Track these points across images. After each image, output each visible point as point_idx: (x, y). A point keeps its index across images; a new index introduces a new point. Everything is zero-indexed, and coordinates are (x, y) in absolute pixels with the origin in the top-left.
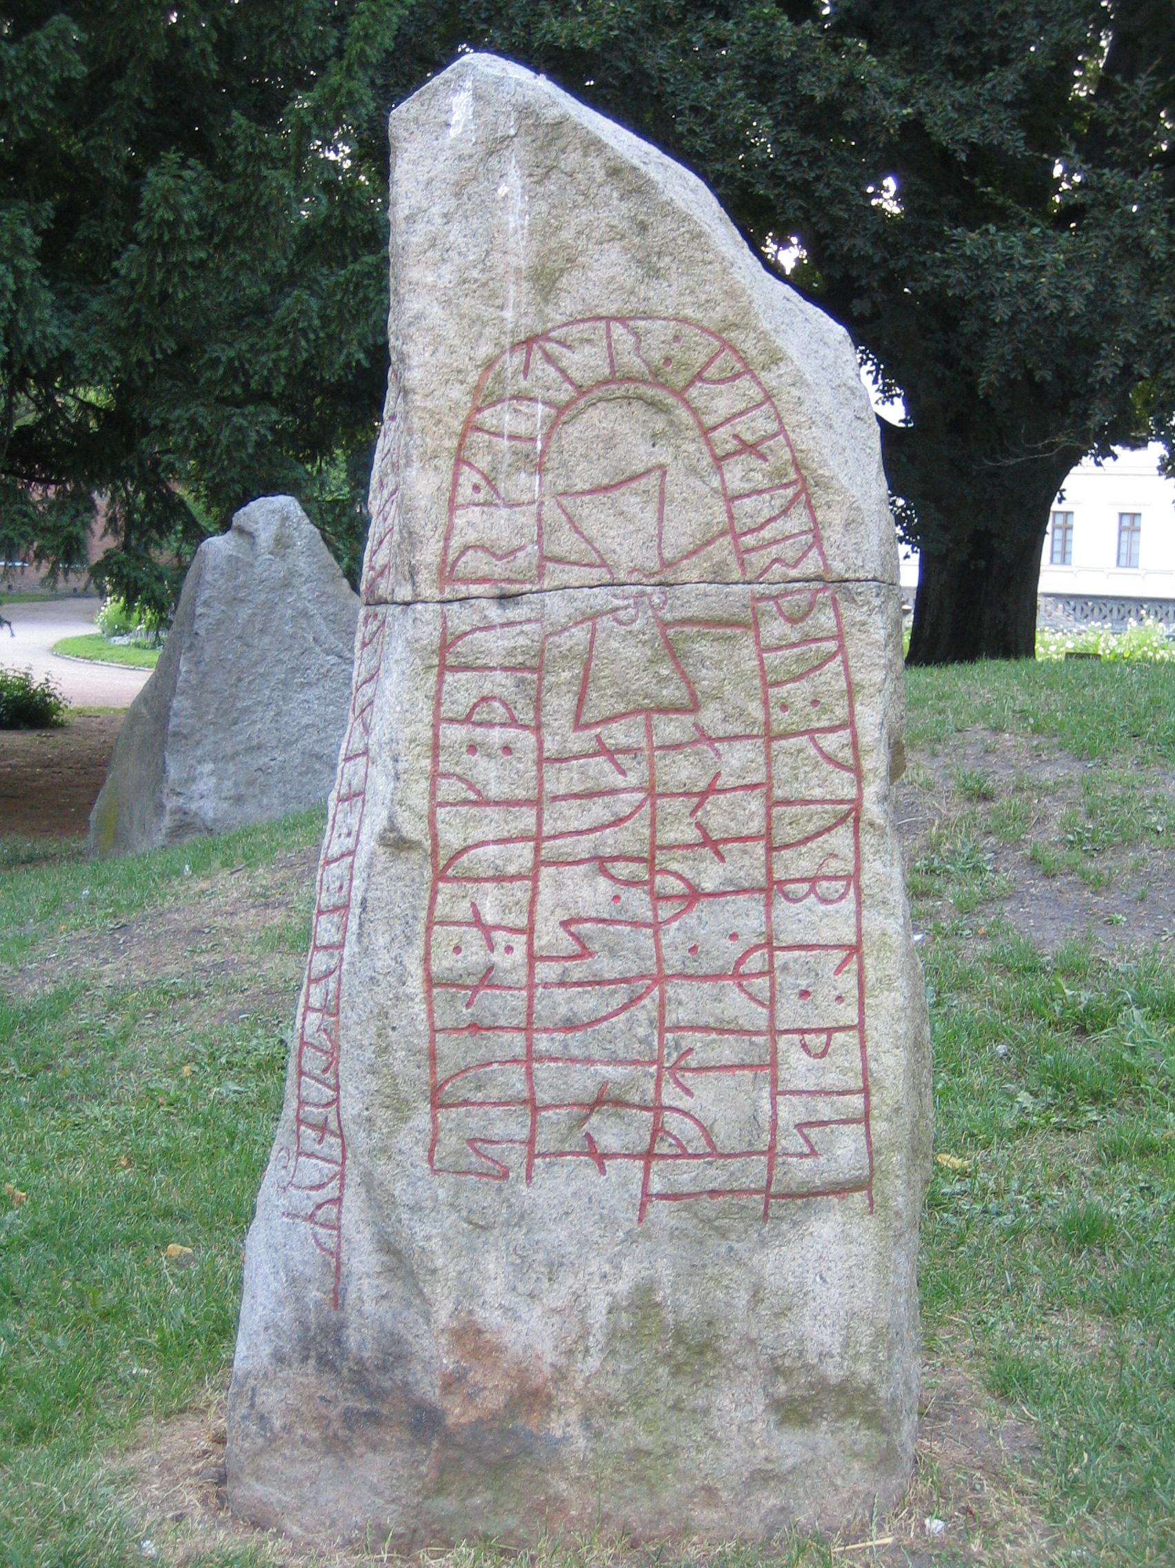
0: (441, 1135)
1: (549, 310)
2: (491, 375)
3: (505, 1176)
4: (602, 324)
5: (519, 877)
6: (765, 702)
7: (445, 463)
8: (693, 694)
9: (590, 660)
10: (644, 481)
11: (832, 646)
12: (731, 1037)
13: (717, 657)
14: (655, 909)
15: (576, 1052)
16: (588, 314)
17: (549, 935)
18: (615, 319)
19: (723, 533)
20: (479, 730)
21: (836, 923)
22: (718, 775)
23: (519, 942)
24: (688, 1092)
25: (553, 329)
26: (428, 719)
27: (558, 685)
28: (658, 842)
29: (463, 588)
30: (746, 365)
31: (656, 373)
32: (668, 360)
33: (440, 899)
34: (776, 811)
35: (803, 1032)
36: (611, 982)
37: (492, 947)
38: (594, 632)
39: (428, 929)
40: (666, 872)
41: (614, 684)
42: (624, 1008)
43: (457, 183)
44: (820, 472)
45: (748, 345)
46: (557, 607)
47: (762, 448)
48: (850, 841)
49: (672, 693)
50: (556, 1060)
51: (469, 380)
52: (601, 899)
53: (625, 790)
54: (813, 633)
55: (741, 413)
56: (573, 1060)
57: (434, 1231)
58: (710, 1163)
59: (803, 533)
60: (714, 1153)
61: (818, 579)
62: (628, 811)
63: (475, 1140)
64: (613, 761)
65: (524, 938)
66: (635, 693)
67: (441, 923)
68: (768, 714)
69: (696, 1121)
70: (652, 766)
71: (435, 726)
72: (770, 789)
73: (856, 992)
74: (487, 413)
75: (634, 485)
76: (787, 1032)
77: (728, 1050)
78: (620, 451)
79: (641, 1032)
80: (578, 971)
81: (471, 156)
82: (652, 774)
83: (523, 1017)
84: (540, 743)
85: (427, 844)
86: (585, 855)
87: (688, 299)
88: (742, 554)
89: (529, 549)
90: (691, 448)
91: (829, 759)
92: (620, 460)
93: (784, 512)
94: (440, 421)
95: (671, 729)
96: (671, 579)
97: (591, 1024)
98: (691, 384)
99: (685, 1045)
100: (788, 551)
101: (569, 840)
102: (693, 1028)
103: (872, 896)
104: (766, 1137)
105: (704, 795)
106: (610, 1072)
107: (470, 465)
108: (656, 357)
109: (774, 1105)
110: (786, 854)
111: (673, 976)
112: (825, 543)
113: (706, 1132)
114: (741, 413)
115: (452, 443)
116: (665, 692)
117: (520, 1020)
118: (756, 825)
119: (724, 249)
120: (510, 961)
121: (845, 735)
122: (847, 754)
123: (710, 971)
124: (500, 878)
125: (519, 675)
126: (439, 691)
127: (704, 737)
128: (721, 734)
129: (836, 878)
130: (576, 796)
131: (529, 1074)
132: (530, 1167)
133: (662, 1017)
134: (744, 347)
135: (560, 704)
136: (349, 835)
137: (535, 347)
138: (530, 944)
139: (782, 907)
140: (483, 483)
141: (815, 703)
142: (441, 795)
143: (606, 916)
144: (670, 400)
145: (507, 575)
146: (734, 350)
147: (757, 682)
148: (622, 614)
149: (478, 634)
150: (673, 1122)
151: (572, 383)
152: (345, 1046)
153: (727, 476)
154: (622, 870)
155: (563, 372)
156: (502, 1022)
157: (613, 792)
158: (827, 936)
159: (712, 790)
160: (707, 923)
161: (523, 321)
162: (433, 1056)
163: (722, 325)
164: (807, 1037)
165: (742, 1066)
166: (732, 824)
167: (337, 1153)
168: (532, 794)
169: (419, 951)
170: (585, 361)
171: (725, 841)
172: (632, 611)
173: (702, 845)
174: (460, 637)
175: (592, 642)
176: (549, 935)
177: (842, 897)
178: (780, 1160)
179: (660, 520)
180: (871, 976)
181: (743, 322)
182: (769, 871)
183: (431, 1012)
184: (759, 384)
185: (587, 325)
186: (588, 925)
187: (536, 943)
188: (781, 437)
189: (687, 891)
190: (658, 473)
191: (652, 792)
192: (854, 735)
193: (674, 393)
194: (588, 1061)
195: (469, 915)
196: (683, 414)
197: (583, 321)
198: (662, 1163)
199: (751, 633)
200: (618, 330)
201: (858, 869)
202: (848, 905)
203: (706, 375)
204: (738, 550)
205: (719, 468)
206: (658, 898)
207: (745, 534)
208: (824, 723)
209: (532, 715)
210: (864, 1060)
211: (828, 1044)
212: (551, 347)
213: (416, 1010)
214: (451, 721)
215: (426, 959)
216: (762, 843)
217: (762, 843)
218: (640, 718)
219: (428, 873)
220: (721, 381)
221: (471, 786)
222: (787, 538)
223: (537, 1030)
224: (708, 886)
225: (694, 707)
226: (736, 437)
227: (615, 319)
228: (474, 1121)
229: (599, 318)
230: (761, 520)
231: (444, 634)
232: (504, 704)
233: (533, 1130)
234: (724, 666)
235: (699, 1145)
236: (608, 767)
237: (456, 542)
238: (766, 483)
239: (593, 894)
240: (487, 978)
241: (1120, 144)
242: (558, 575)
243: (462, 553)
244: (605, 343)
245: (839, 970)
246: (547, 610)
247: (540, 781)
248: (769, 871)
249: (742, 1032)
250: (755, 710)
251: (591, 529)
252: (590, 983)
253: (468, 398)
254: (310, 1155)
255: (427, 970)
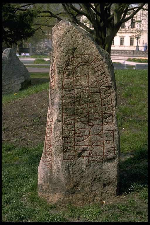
136: (51, 119)
152: (52, 145)
167: (51, 158)
194: (82, 145)
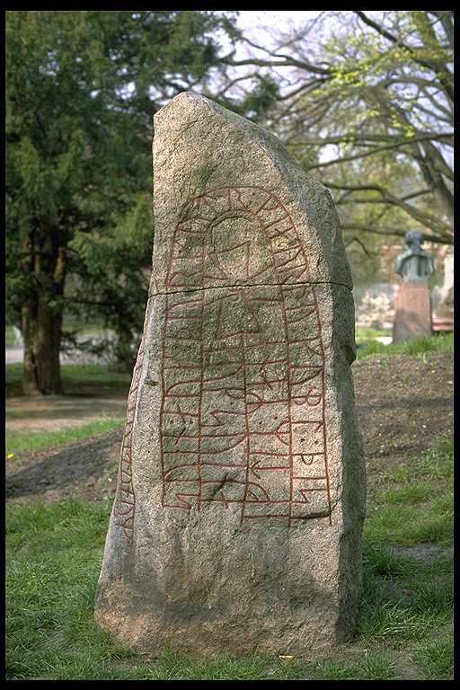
7: (169, 242)
11: (313, 307)
56: (216, 464)
133: (249, 448)
158: (311, 417)
160: (265, 412)
167: (132, 500)
194: (221, 465)
198: (250, 505)
224: (266, 399)
240: (183, 433)
241: (117, 62)
254: (125, 502)
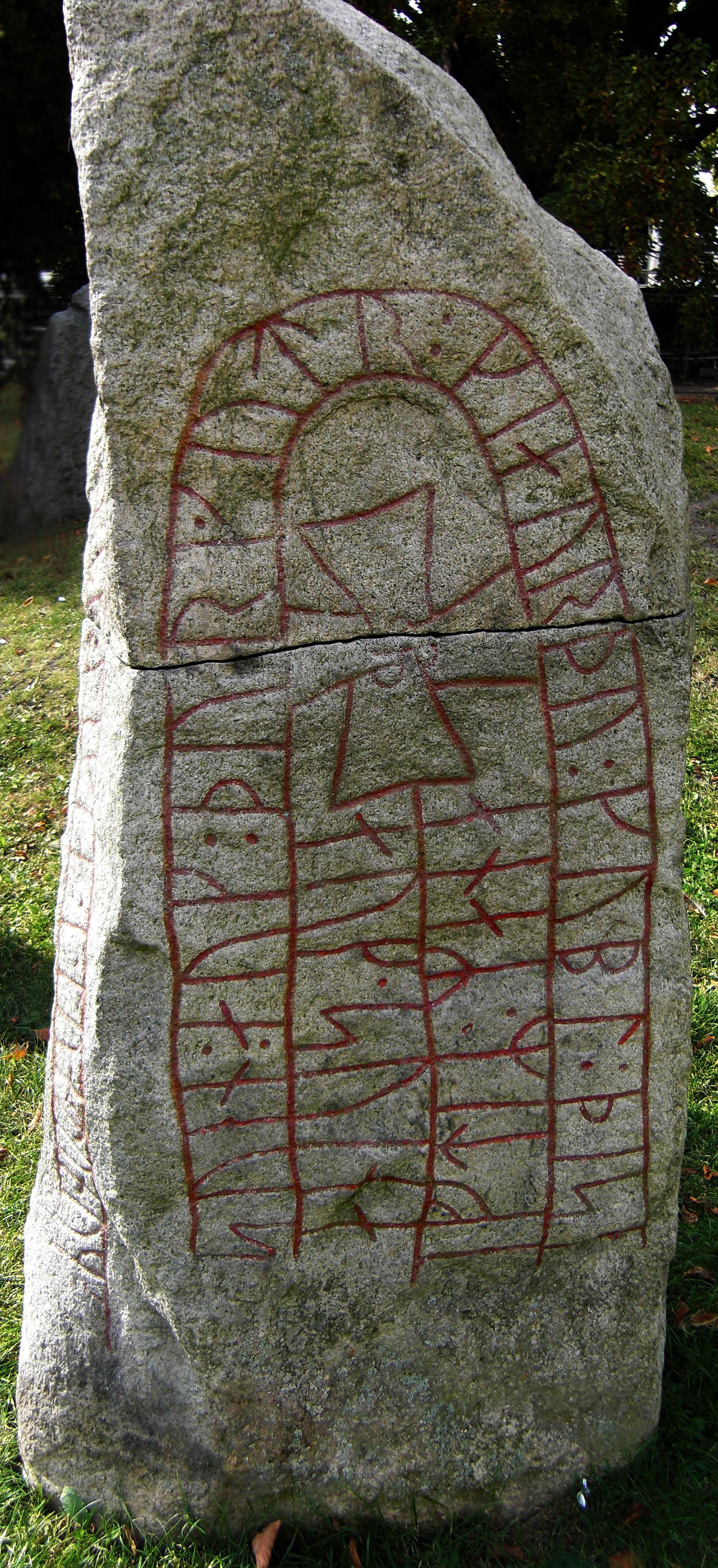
0: (202, 1224)
1: (282, 283)
2: (212, 375)
3: (272, 1253)
4: (352, 300)
5: (273, 971)
6: (552, 767)
7: (160, 492)
8: (468, 760)
9: (346, 731)
10: (406, 504)
11: (630, 697)
12: (507, 1110)
13: (497, 719)
14: (425, 990)
15: (340, 1135)
16: (333, 286)
17: (310, 1023)
18: (367, 292)
19: (504, 569)
20: (218, 817)
21: (622, 990)
22: (498, 850)
23: (276, 1036)
24: (462, 1165)
25: (289, 308)
26: (157, 809)
27: (310, 761)
28: (429, 923)
29: (190, 651)
30: (534, 352)
31: (421, 363)
32: (436, 347)
33: (184, 1001)
34: (561, 884)
35: (582, 1099)
36: (377, 1064)
37: (245, 1043)
38: (349, 697)
39: (174, 1034)
40: (437, 949)
41: (376, 756)
42: (393, 1087)
43: (154, 106)
44: (624, 490)
45: (540, 329)
46: (305, 667)
47: (554, 460)
48: (640, 906)
49: (444, 761)
50: (321, 1145)
51: (184, 382)
52: (364, 984)
53: (389, 872)
54: (609, 684)
55: (528, 416)
57: (200, 1314)
58: (484, 1227)
59: (599, 562)
60: (489, 1215)
61: (619, 619)
62: (394, 894)
63: (239, 1224)
64: (377, 841)
65: (281, 1030)
66: (400, 764)
67: (188, 1025)
68: (555, 781)
69: (472, 1192)
70: (421, 844)
71: (166, 817)
72: (556, 859)
73: (640, 1060)
74: (208, 424)
75: (395, 509)
76: (565, 1102)
77: (503, 1122)
78: (376, 468)
79: (412, 1113)
80: (343, 1056)
81: (171, 65)
82: (422, 854)
83: (284, 1107)
84: (290, 826)
85: (166, 947)
86: (346, 942)
87: (461, 264)
88: (527, 594)
89: (268, 597)
90: (464, 460)
91: (622, 823)
92: (378, 478)
93: (579, 537)
94: (148, 438)
95: (443, 801)
96: (442, 629)
97: (357, 1105)
98: (465, 377)
99: (458, 1123)
100: (581, 585)
101: (327, 930)
102: (466, 1106)
103: (661, 961)
104: (543, 1201)
105: (480, 872)
106: (377, 1153)
107: (190, 492)
108: (421, 342)
109: (551, 1172)
110: (570, 925)
111: (445, 1056)
112: (626, 574)
113: (481, 1200)
114: (528, 416)
115: (166, 466)
116: (435, 762)
117: (281, 1109)
118: (539, 900)
119: (505, 194)
120: (268, 1052)
121: (642, 797)
122: (642, 819)
123: (485, 1049)
124: (250, 974)
125: (263, 752)
126: (168, 774)
127: (481, 808)
128: (500, 804)
129: (623, 944)
130: (337, 880)
131: (293, 1160)
132: (297, 1243)
134: (533, 328)
135: (312, 785)
137: (266, 332)
138: (288, 1035)
139: (565, 980)
140: (208, 515)
141: (609, 763)
142: (177, 894)
143: (372, 1001)
144: (439, 399)
145: (243, 631)
146: (521, 334)
147: (543, 745)
148: (384, 674)
149: (211, 708)
150: (445, 1194)
151: (315, 381)
153: (510, 495)
154: (387, 952)
155: (302, 365)
156: (261, 1114)
157: (378, 874)
158: (613, 1007)
159: (489, 866)
161: (249, 299)
162: (187, 1157)
163: (504, 299)
164: (587, 1104)
165: (518, 1136)
166: (512, 900)
168: (282, 884)
169: (164, 1058)
170: (332, 351)
171: (503, 916)
172: (396, 669)
173: (479, 921)
174: (188, 712)
175: (348, 711)
176: (310, 1023)
177: (629, 964)
178: (557, 1220)
179: (428, 552)
180: (657, 1042)
181: (534, 295)
182: (551, 942)
183: (181, 1117)
184: (551, 377)
185: (332, 301)
186: (352, 1012)
187: (295, 1034)
188: (577, 446)
189: (460, 967)
190: (424, 494)
191: (421, 870)
192: (652, 797)
193: (444, 388)
194: (355, 1143)
195: (219, 1016)
196: (455, 417)
197: (327, 295)
199: (537, 689)
200: (372, 308)
201: (648, 933)
202: (634, 974)
203: (484, 365)
204: (522, 587)
205: (500, 484)
206: (427, 976)
207: (531, 569)
208: (619, 784)
209: (279, 796)
210: (646, 1122)
211: (609, 1110)
212: (286, 332)
213: (165, 1115)
214: (184, 808)
215: (173, 1064)
216: (545, 917)
217: (545, 917)
218: (407, 791)
219: (168, 976)
220: (504, 373)
221: (212, 882)
222: (581, 570)
223: (300, 1117)
224: (484, 960)
225: (469, 774)
226: (522, 446)
227: (367, 292)
228: (238, 1208)
229: (346, 291)
230: (551, 550)
231: (169, 707)
232: (246, 786)
233: (299, 1211)
234: (510, 732)
235: (475, 1211)
236: (371, 848)
237: (177, 594)
238: (557, 503)
239: (358, 981)
240: (243, 1073)
242: (305, 628)
243: (186, 608)
244: (354, 327)
245: (624, 1039)
246: (293, 674)
247: (292, 868)
248: (551, 942)
249: (519, 1103)
250: (540, 777)
251: (345, 570)
252: (355, 1068)
253: (183, 406)
255: (175, 1077)
